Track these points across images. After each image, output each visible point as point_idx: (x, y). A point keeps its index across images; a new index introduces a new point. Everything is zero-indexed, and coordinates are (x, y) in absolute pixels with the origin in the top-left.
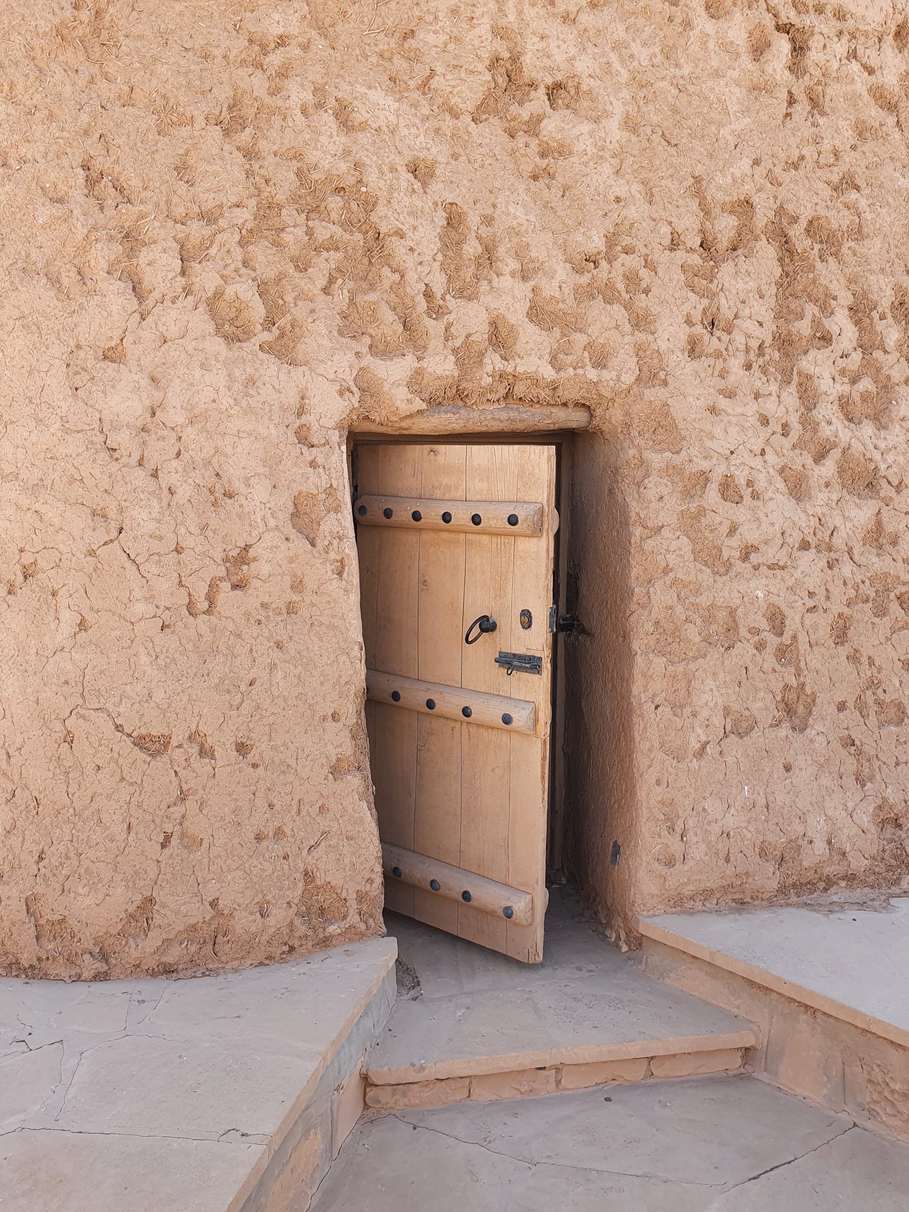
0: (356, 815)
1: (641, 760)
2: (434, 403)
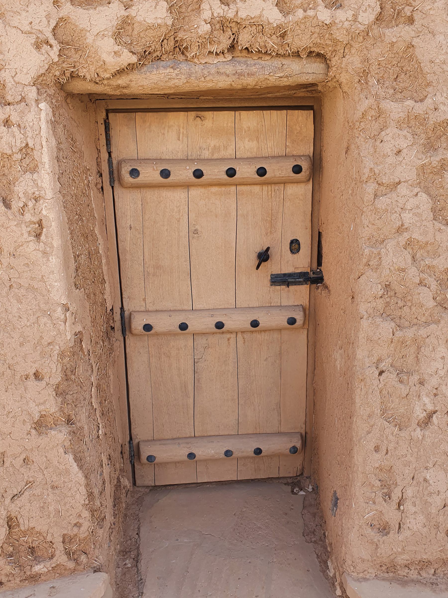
0: (61, 467)
1: (360, 426)
2: (147, 57)
